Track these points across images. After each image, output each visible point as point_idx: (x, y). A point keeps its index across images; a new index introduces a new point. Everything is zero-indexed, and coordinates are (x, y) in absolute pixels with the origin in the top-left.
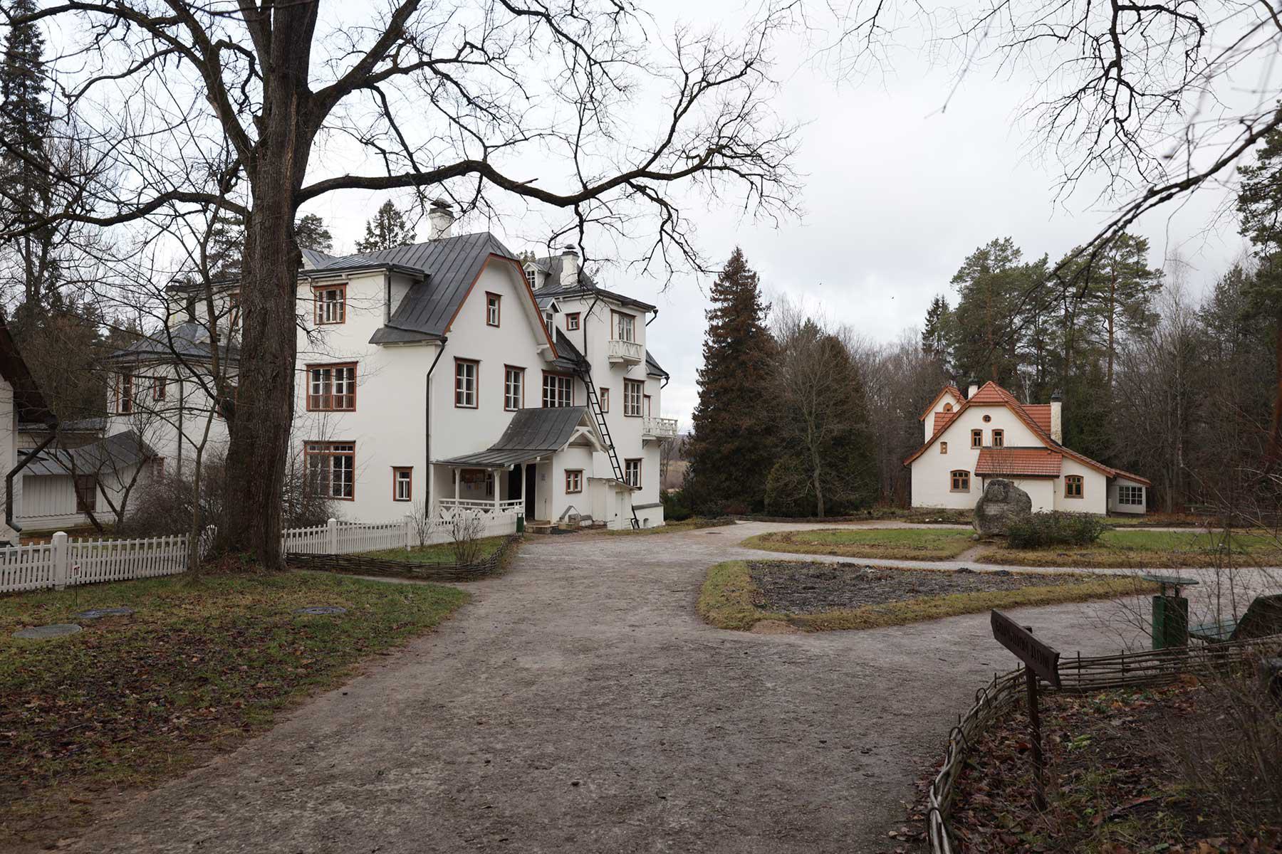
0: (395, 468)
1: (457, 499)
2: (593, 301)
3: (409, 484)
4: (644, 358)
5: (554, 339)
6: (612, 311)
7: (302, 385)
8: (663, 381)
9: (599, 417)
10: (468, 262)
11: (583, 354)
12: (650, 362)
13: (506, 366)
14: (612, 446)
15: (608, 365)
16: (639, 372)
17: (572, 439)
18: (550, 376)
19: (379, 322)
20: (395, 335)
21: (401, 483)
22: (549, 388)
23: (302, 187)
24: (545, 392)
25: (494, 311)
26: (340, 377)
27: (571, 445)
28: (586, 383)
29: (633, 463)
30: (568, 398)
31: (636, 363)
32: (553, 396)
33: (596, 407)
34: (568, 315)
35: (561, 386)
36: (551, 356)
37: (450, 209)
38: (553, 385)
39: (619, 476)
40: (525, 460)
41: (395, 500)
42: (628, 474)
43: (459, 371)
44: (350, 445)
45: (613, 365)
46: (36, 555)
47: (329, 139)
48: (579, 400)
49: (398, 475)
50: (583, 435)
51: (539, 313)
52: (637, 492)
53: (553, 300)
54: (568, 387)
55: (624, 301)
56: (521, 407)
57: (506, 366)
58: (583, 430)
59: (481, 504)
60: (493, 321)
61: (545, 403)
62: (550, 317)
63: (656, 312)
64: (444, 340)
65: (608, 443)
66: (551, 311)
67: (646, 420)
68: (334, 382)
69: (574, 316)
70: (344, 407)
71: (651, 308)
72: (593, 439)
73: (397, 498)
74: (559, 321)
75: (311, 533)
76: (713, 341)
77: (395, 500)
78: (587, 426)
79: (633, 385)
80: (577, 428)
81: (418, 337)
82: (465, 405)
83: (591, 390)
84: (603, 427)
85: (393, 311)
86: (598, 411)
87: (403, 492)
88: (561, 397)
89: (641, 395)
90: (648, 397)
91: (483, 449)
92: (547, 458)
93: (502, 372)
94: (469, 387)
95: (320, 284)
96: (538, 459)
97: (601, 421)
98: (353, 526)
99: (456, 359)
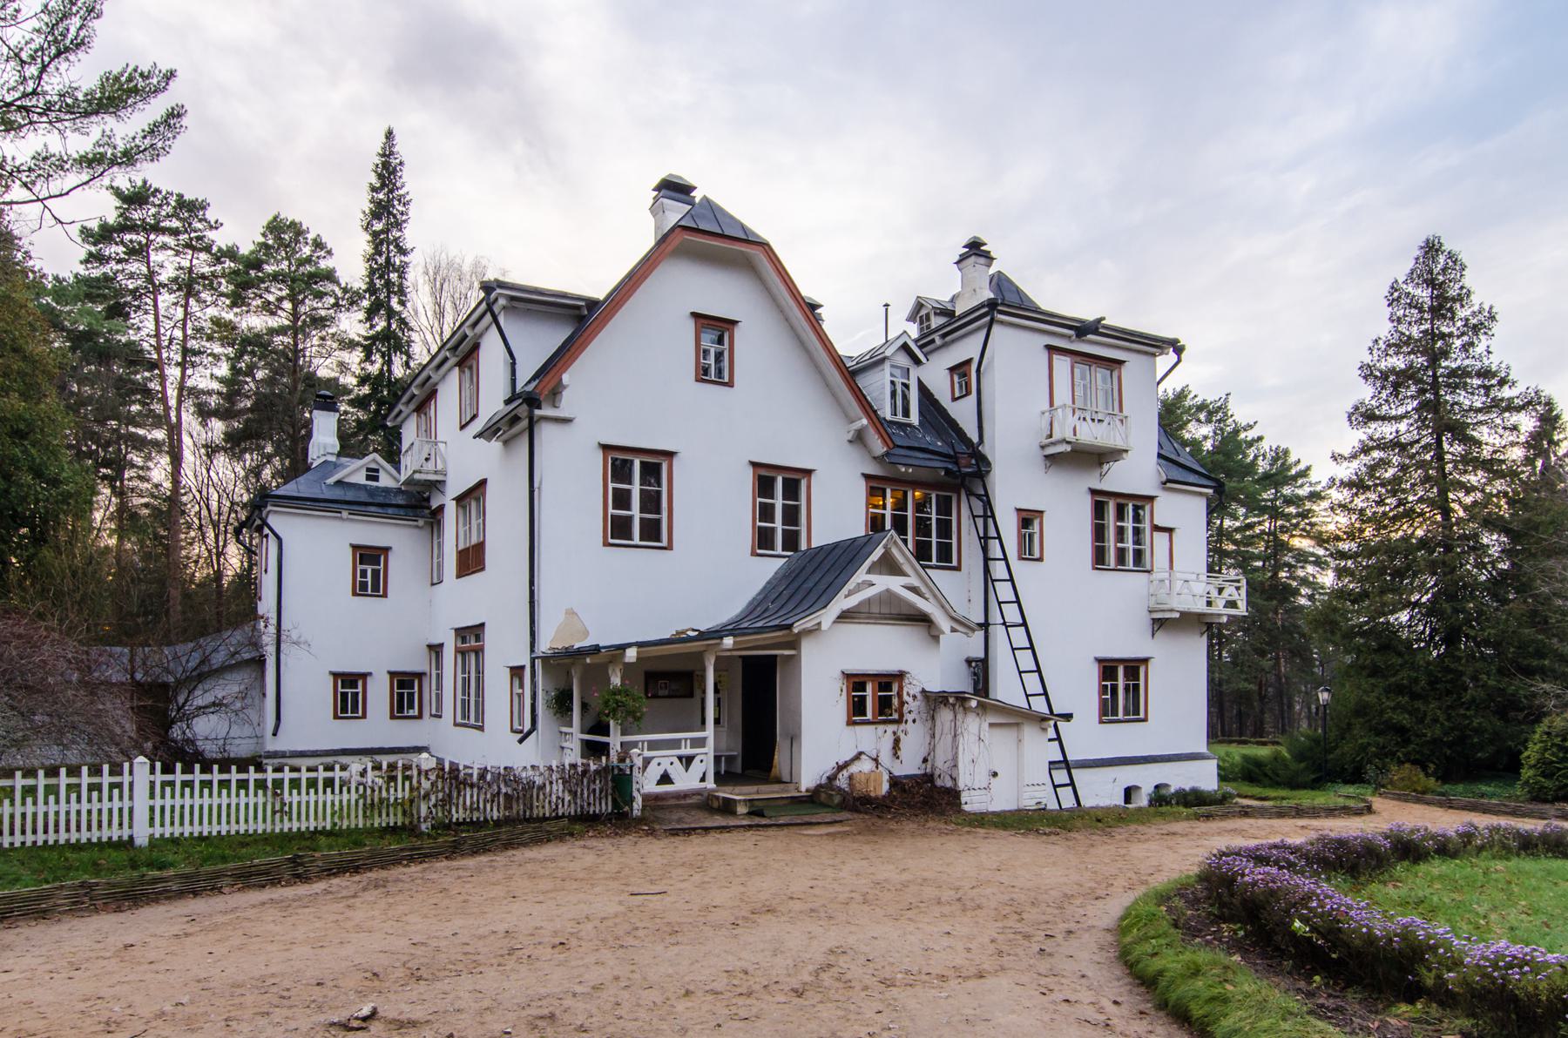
2: (982, 335)
6: (1051, 349)
15: (1040, 461)
17: (841, 603)
26: (1120, 515)
27: (845, 616)
43: (764, 485)
59: (676, 744)
63: (1179, 350)
73: (459, 720)
77: (456, 725)
89: (1147, 526)
90: (1170, 530)
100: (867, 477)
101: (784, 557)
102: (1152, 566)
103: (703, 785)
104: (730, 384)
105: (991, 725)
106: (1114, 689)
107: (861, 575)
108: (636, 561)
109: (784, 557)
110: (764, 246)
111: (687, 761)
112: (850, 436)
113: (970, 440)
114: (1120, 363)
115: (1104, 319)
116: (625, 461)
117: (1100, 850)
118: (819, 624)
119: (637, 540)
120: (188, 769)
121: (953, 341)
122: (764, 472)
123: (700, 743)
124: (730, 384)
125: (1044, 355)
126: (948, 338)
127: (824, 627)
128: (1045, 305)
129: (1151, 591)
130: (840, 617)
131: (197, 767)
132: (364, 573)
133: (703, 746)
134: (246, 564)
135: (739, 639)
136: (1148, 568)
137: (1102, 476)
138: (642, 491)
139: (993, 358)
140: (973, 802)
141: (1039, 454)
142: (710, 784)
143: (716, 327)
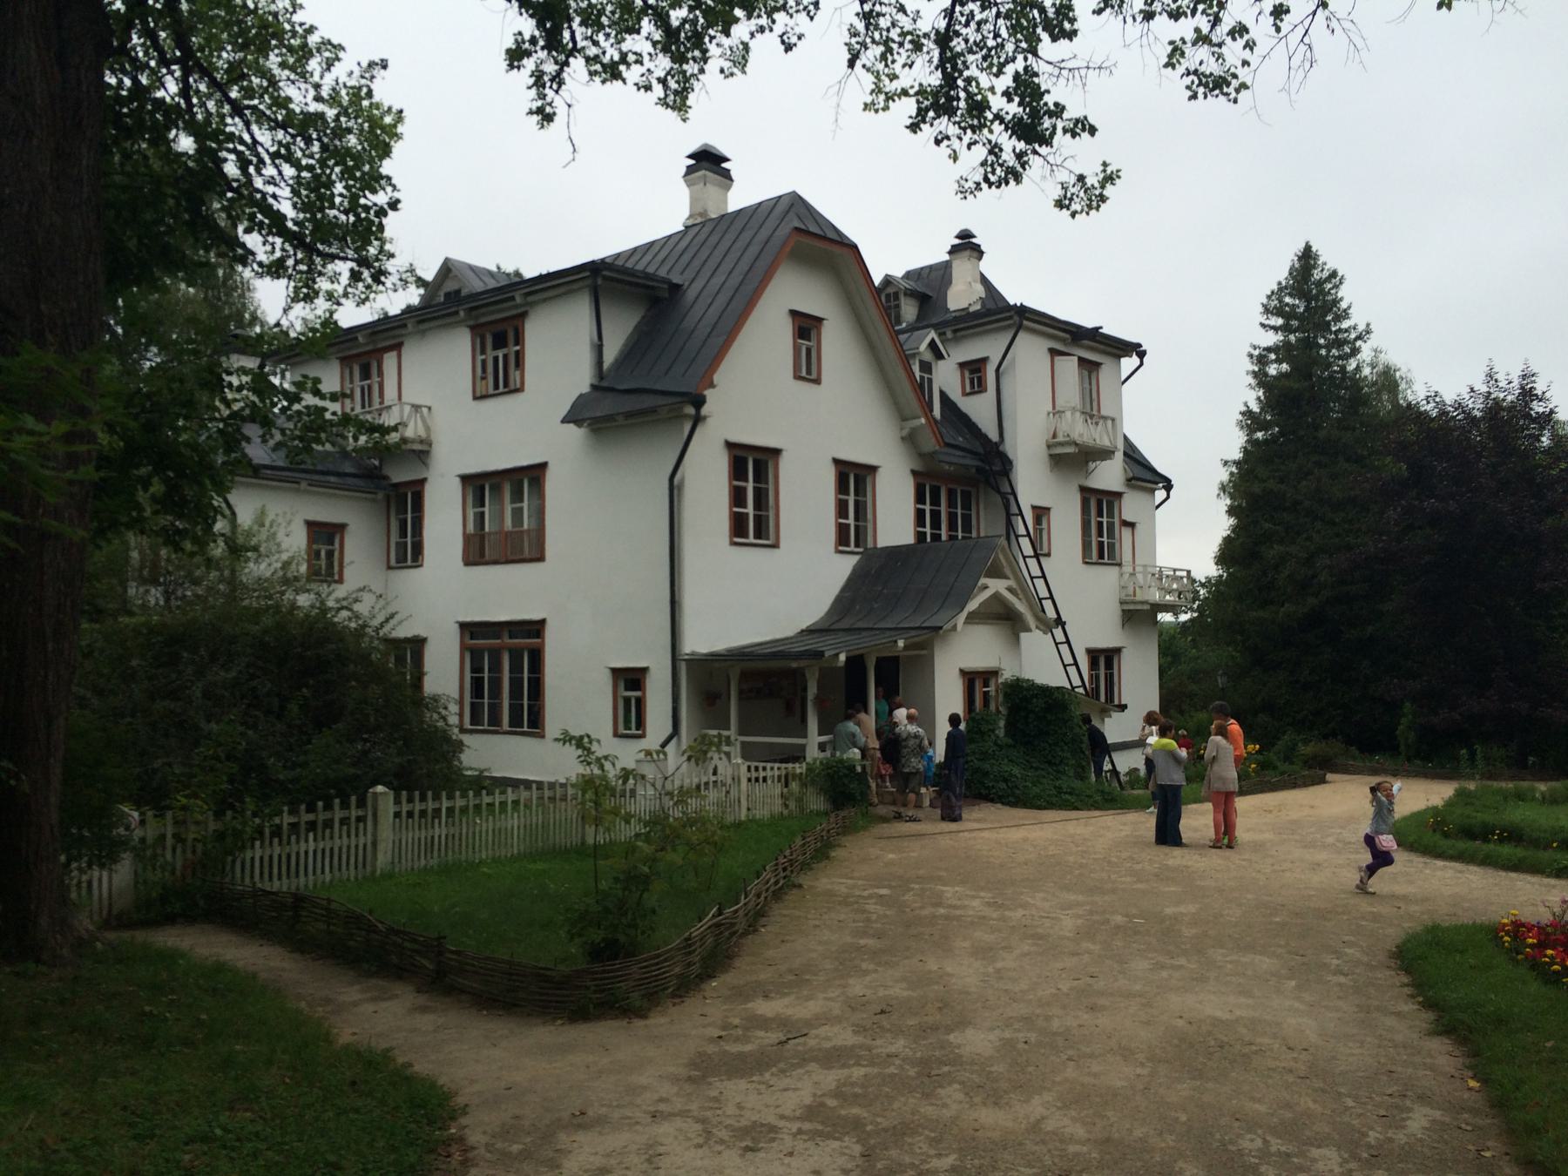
0: (616, 672)
1: (732, 732)
3: (640, 703)
4: (1121, 445)
5: (937, 412)
7: (517, 529)
8: (1160, 495)
9: (1032, 563)
10: (754, 250)
11: (993, 435)
12: (1133, 456)
13: (837, 462)
14: (1059, 622)
15: (1046, 459)
16: (1109, 475)
17: (973, 605)
18: (927, 485)
19: (581, 380)
20: (607, 406)
21: (627, 700)
22: (927, 508)
24: (920, 515)
25: (809, 351)
27: (973, 618)
28: (1004, 496)
29: (1103, 659)
30: (967, 528)
31: (1106, 454)
32: (936, 524)
33: (1025, 543)
34: (962, 365)
35: (952, 503)
36: (930, 443)
37: (725, 165)
38: (936, 501)
39: (1076, 682)
40: (872, 646)
41: (616, 735)
42: (1095, 678)
44: (536, 628)
48: (987, 524)
49: (622, 685)
51: (906, 359)
52: (1115, 715)
53: (932, 335)
54: (967, 506)
56: (870, 545)
57: (837, 462)
58: (997, 586)
60: (807, 369)
61: (920, 537)
62: (926, 367)
63: (1142, 355)
65: (1051, 613)
66: (928, 356)
67: (1127, 569)
71: (1137, 350)
72: (1020, 606)
73: (622, 730)
74: (947, 377)
75: (765, 779)
79: (1098, 504)
80: (983, 581)
81: (648, 401)
82: (751, 540)
83: (1014, 510)
84: (1040, 583)
85: (609, 357)
86: (1028, 550)
87: (631, 717)
88: (952, 526)
89: (1116, 520)
90: (1132, 525)
93: (829, 477)
95: (483, 320)
96: (901, 643)
97: (1036, 571)
99: (730, 445)
102: (1050, 550)
104: (817, 381)
106: (1097, 677)
108: (752, 558)
110: (854, 248)
112: (905, 432)
113: (985, 437)
114: (1097, 365)
115: (1101, 328)
118: (956, 625)
119: (751, 540)
120: (478, 794)
122: (739, 453)
124: (817, 381)
125: (1046, 359)
126: (959, 334)
129: (1122, 584)
132: (318, 554)
136: (1118, 561)
137: (1088, 474)
138: (754, 488)
139: (1014, 359)
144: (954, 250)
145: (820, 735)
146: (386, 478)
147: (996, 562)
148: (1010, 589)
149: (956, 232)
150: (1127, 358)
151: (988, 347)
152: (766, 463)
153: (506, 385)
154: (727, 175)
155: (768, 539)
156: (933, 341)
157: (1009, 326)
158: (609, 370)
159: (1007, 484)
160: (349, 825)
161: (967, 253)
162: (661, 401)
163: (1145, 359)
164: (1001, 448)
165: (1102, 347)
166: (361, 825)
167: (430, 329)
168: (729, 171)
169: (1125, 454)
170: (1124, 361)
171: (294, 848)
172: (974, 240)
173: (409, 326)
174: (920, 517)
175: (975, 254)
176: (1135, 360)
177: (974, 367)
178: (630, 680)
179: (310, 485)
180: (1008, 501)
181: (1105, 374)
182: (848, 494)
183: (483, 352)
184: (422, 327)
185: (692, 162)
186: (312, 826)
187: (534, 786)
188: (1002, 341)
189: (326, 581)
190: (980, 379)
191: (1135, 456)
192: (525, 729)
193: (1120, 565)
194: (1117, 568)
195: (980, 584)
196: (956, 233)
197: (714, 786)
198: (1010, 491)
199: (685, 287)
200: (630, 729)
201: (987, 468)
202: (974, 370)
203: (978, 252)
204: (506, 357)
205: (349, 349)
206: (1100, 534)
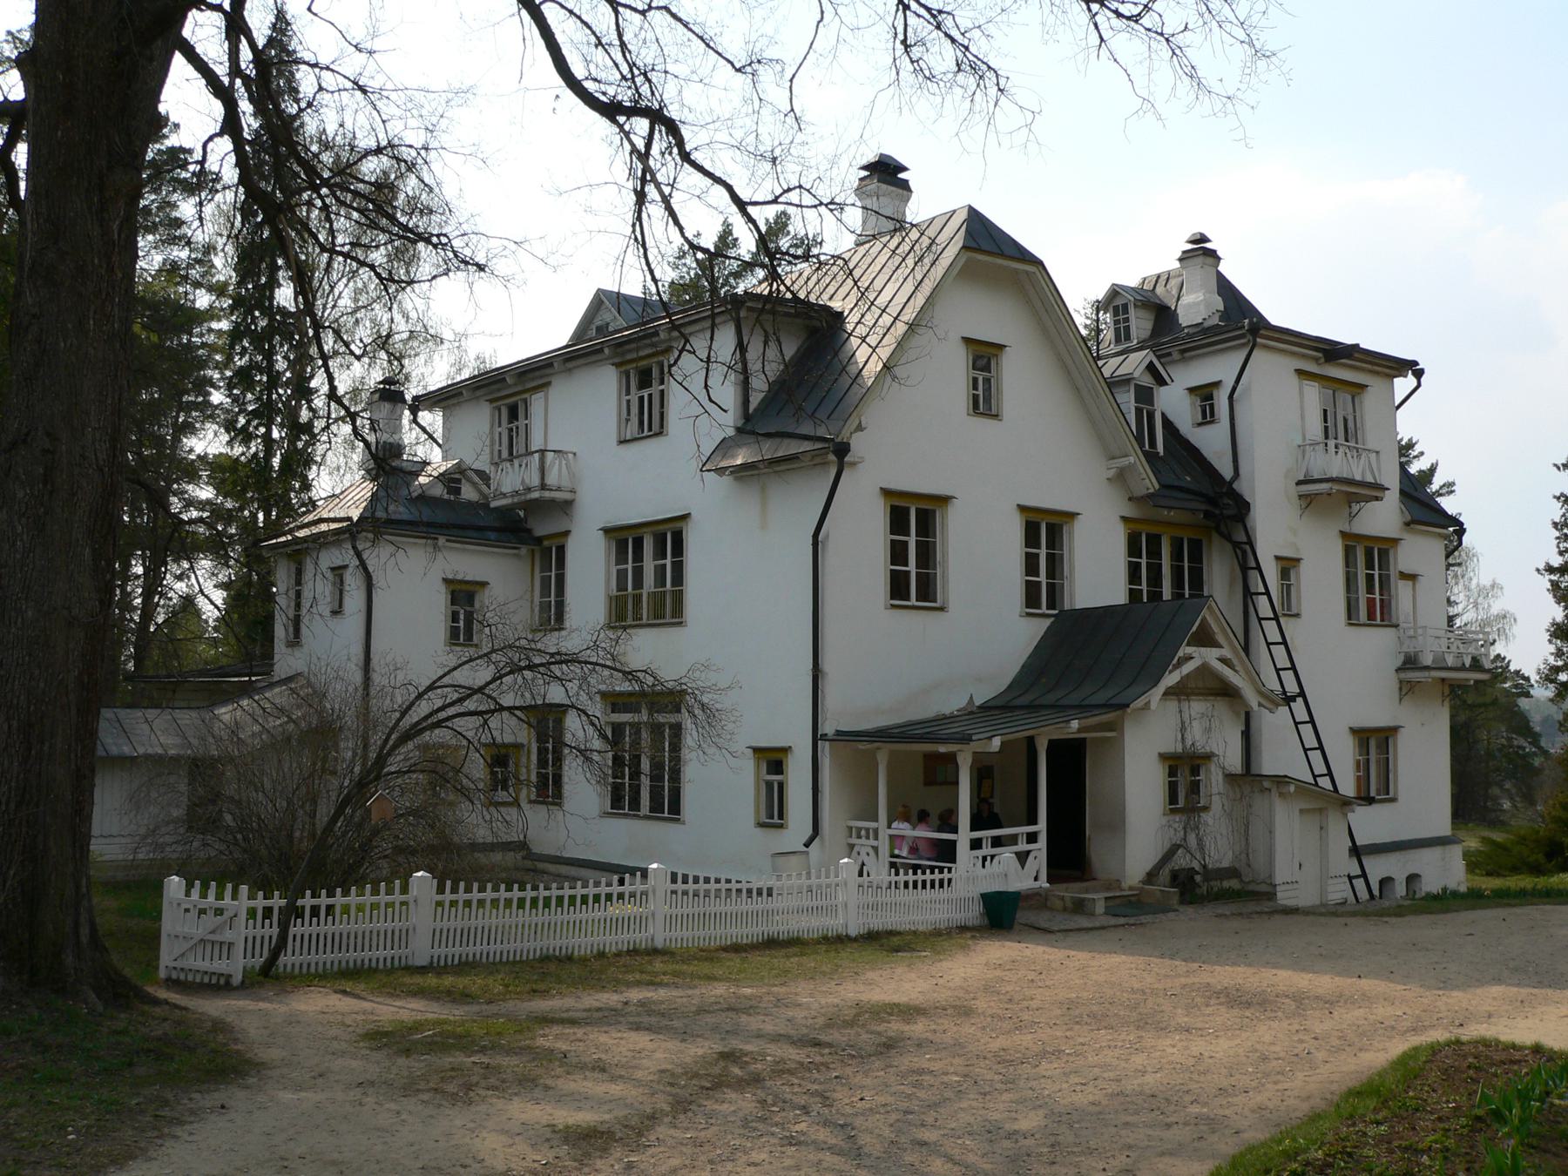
9: (1270, 627)
11: (1226, 472)
13: (1023, 509)
16: (1382, 518)
17: (1171, 679)
21: (769, 785)
23: (177, 52)
34: (1192, 390)
36: (1147, 482)
37: (901, 176)
43: (898, 521)
45: (1308, 502)
46: (674, 896)
47: (1003, 99)
50: (1204, 669)
55: (1332, 351)
60: (984, 403)
61: (1134, 595)
63: (1419, 374)
64: (842, 450)
68: (649, 565)
69: (1204, 394)
70: (644, 621)
76: (219, 281)
78: (1217, 645)
80: (1185, 650)
82: (1378, 622)
90: (1412, 577)
91: (953, 703)
92: (1110, 726)
94: (1051, 573)
98: (723, 886)
100: (1124, 519)
101: (1048, 616)
103: (1037, 884)
105: (1301, 811)
107: (1185, 650)
108: (913, 623)
109: (1048, 616)
110: (1039, 263)
111: (1022, 857)
112: (1111, 473)
114: (1363, 387)
116: (926, 511)
117: (843, 954)
118: (1148, 704)
119: (913, 601)
121: (1192, 358)
123: (1032, 838)
127: (1153, 706)
128: (1275, 319)
130: (1165, 694)
131: (516, 886)
133: (1035, 841)
134: (1524, 790)
135: (1083, 721)
137: (1352, 517)
140: (1284, 897)
141: (1294, 491)
142: (1043, 883)
143: (984, 355)
144: (1185, 257)
145: (972, 830)
146: (529, 531)
147: (1204, 625)
148: (1223, 660)
149: (1187, 236)
150: (1401, 378)
151: (1219, 368)
152: (934, 511)
153: (650, 429)
154: (905, 185)
155: (935, 601)
156: (1151, 362)
157: (1243, 345)
158: (756, 410)
159: (1243, 533)
160: (470, 907)
161: (1200, 259)
162: (806, 446)
163: (1422, 380)
164: (1235, 486)
165: (1369, 366)
166: (453, 909)
167: (578, 367)
168: (907, 181)
169: (1402, 492)
170: (1398, 381)
171: (521, 919)
172: (1208, 245)
173: (555, 364)
174: (1134, 572)
175: (1210, 260)
176: (1411, 381)
177: (1206, 391)
178: (773, 760)
179: (448, 541)
180: (1244, 553)
181: (1370, 400)
182: (1039, 547)
183: (628, 393)
184: (569, 365)
185: (865, 173)
186: (621, 896)
187: (639, 873)
188: (1236, 359)
189: (556, 630)
190: (1212, 406)
191: (1415, 494)
192: (666, 815)
193: (1396, 626)
194: (1394, 629)
195: (1180, 653)
196: (1186, 238)
197: (519, 907)
198: (1245, 540)
199: (845, 314)
200: (773, 818)
201: (1217, 512)
202: (1204, 394)
203: (1213, 255)
204: (650, 395)
205: (499, 390)
206: (1370, 590)
